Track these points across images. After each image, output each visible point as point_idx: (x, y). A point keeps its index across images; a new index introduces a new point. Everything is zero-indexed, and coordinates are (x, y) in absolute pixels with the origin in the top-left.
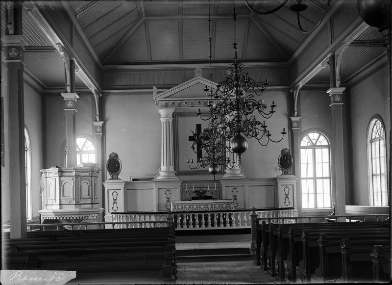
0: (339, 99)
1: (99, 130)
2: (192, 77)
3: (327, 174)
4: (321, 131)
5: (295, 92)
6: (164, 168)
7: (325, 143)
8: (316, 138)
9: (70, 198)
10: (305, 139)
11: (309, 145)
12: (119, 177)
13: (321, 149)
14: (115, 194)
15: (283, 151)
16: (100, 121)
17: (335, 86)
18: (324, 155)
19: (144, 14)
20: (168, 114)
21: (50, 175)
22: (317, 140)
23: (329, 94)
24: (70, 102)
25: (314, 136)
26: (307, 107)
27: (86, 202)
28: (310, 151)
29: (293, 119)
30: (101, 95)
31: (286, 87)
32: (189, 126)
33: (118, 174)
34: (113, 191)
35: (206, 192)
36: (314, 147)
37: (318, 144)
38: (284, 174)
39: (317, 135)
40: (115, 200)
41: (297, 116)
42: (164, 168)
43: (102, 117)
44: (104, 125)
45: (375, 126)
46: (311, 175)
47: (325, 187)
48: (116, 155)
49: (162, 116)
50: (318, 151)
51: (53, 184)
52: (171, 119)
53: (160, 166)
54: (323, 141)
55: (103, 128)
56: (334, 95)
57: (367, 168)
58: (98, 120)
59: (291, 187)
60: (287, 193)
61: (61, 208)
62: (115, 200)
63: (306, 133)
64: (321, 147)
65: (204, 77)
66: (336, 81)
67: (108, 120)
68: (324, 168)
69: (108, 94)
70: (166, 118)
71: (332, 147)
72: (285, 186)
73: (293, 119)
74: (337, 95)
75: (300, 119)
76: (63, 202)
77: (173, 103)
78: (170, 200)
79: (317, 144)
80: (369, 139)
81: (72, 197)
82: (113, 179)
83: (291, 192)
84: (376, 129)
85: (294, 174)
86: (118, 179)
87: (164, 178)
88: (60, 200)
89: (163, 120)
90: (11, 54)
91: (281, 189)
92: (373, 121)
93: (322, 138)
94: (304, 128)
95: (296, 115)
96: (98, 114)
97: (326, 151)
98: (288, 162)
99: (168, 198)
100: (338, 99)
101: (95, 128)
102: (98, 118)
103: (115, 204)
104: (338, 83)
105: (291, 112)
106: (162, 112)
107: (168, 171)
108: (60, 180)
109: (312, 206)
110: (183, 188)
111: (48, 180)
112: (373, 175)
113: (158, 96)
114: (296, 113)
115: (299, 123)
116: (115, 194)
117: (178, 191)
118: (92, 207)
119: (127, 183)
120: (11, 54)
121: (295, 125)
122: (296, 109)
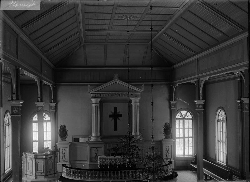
0: (201, 107)
1: (53, 108)
2: (112, 79)
3: (191, 135)
4: (188, 110)
5: (173, 87)
6: (94, 134)
7: (190, 117)
8: (185, 114)
9: (41, 172)
10: (179, 114)
11: (181, 118)
12: (66, 140)
13: (187, 121)
14: (64, 150)
15: (166, 124)
16: (54, 103)
17: (199, 99)
18: (189, 124)
19: (84, 41)
20: (97, 102)
21: (29, 156)
22: (186, 115)
23: (195, 102)
24: (40, 107)
25: (184, 112)
26: (180, 100)
27: (51, 173)
28: (181, 121)
29: (172, 103)
30: (55, 86)
31: (168, 83)
32: (110, 108)
33: (66, 138)
34: (62, 149)
35: (119, 148)
36: (184, 119)
37: (186, 117)
38: (166, 138)
39: (185, 112)
40: (64, 154)
41: (175, 101)
42: (94, 134)
43: (56, 101)
44: (56, 105)
45: (220, 113)
46: (181, 135)
47: (190, 144)
48: (65, 127)
49: (93, 103)
50: (186, 121)
51: (31, 162)
52: (98, 105)
53: (91, 133)
54: (189, 115)
55: (56, 107)
56: (199, 105)
57: (215, 130)
58: (53, 102)
59: (170, 146)
60: (168, 150)
61: (36, 178)
62: (64, 154)
63: (179, 111)
64: (188, 119)
65: (119, 80)
66: (200, 96)
67: (59, 102)
68: (189, 132)
69: (59, 85)
70: (96, 104)
71: (194, 119)
72: (167, 146)
73: (172, 103)
74: (200, 104)
75: (176, 103)
76: (38, 174)
77: (100, 95)
78: (98, 155)
79: (186, 118)
80: (217, 119)
81: (43, 171)
82: (62, 141)
83: (170, 149)
84: (221, 115)
85: (172, 138)
86: (65, 141)
87: (94, 141)
88: (35, 173)
89: (94, 105)
90: (14, 111)
91: (164, 147)
92: (219, 111)
93: (189, 114)
94: (178, 107)
95: (173, 100)
96: (53, 98)
97: (191, 121)
98: (168, 130)
99: (96, 154)
100: (201, 107)
101: (51, 107)
102: (53, 101)
103: (64, 157)
104: (201, 98)
105: (170, 99)
106: (93, 100)
107: (96, 136)
108: (35, 161)
109: (182, 153)
110: (105, 147)
111: (27, 160)
112: (218, 141)
113: (90, 91)
114: (174, 99)
115: (175, 105)
116: (64, 150)
117: (103, 149)
118: (55, 176)
119: (71, 143)
120: (14, 111)
121: (173, 106)
122: (174, 97)
